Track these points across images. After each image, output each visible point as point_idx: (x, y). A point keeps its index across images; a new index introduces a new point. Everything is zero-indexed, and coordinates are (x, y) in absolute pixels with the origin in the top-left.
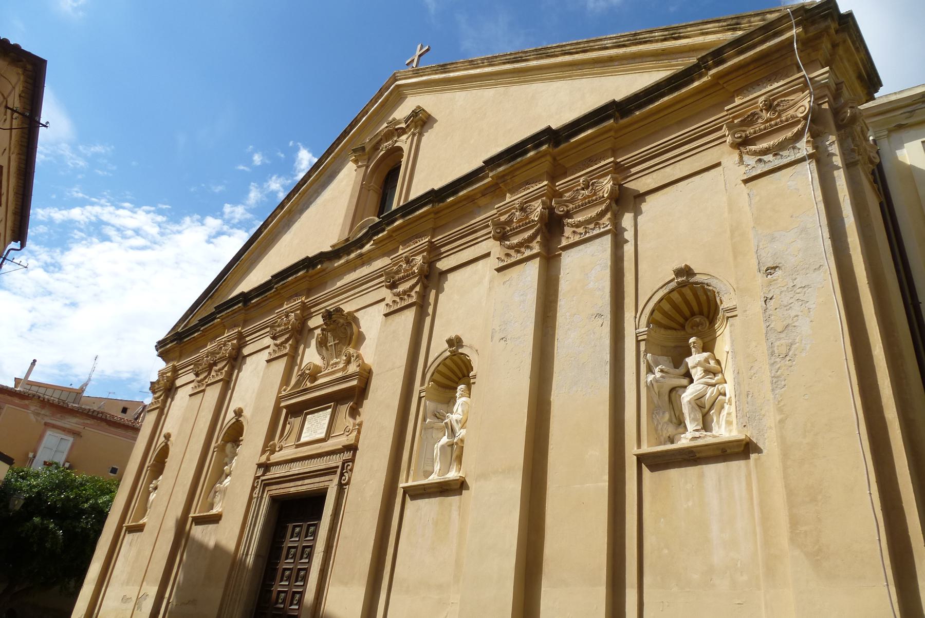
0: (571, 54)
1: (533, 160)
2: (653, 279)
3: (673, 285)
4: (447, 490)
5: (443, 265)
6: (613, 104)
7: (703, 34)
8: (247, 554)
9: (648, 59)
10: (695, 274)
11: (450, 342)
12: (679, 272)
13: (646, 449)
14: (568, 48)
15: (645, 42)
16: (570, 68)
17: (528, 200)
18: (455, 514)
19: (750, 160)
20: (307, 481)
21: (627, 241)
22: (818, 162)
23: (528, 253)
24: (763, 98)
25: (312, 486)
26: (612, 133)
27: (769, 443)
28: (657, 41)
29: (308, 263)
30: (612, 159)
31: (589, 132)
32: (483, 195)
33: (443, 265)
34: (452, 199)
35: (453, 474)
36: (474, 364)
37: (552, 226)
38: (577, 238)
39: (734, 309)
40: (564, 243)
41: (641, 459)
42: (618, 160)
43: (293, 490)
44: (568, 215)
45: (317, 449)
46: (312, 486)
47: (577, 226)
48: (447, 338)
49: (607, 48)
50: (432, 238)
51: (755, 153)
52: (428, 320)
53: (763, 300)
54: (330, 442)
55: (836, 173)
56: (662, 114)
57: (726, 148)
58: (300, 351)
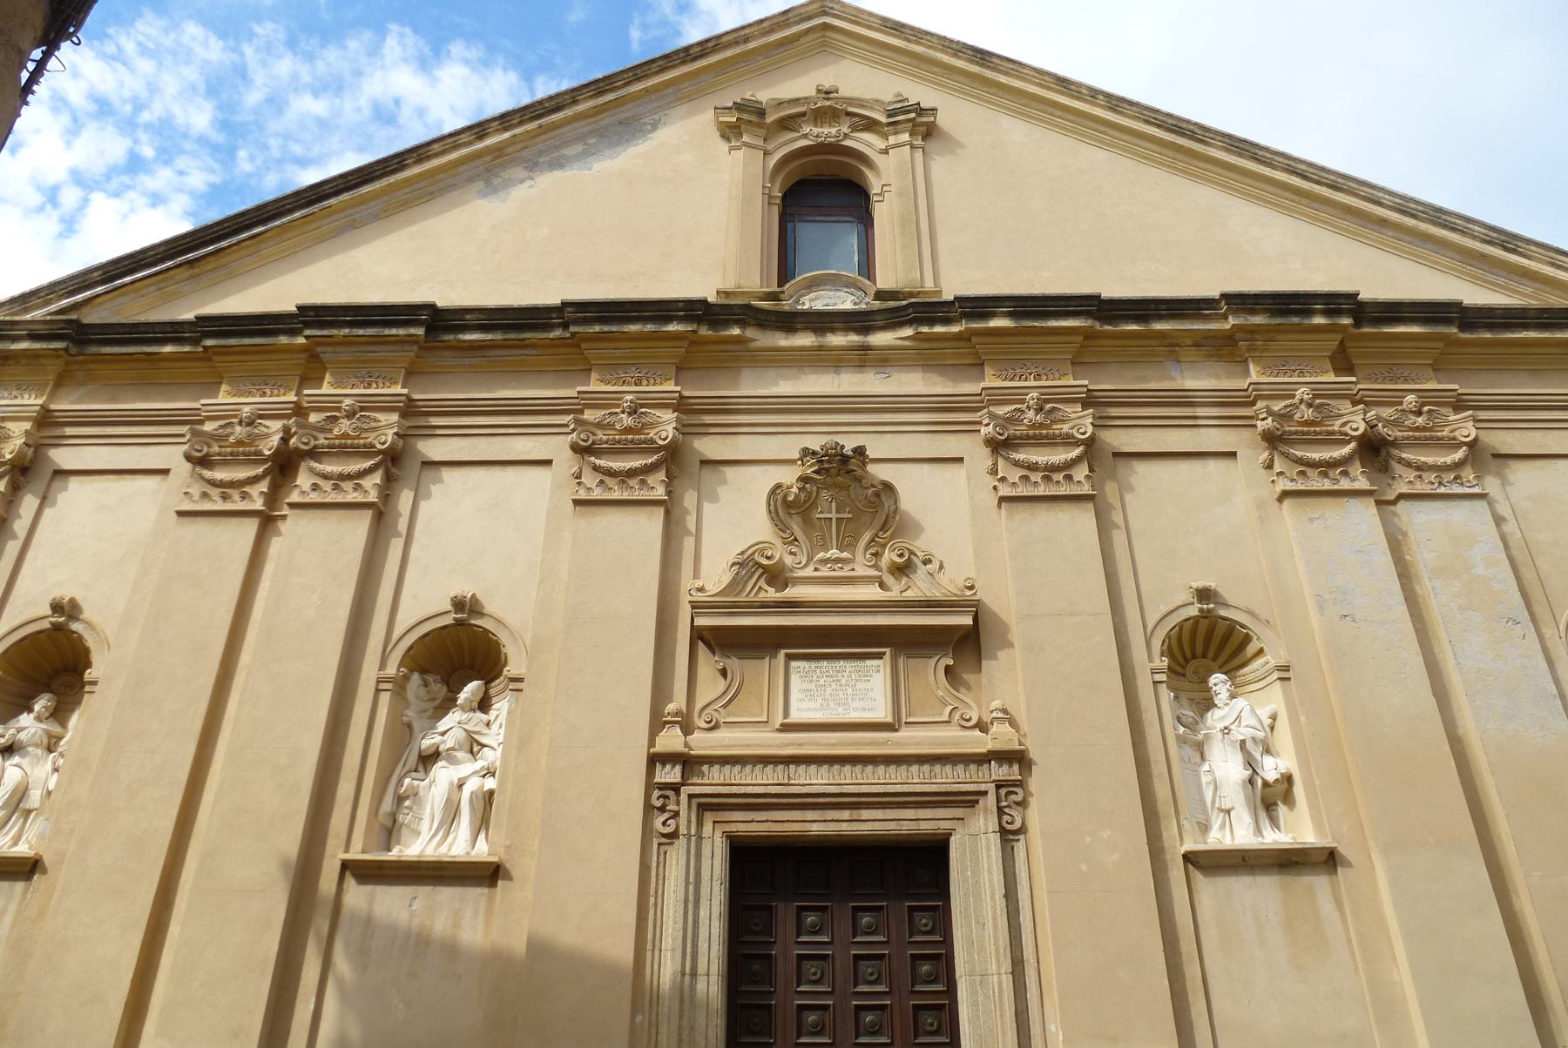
0: (1305, 178)
1: (1318, 329)
2: (422, 599)
3: (45, 625)
4: (1297, 863)
5: (63, 457)
6: (1095, 298)
7: (1553, 265)
8: (694, 974)
9: (1451, 254)
10: (482, 614)
11: (57, 607)
12: (459, 604)
13: (355, 854)
14: (1303, 167)
15: (1453, 229)
16: (1296, 198)
17: (647, 398)
18: (1326, 905)
19: (590, 479)
20: (763, 815)
21: (15, 537)
22: (667, 513)
23: (352, 497)
24: (629, 397)
25: (877, 826)
26: (685, 344)
27: (524, 868)
28: (1474, 238)
29: (438, 322)
30: (405, 391)
31: (1415, 329)
32: (1196, 345)
33: (63, 457)
34: (1135, 327)
35: (482, 851)
36: (95, 658)
37: (284, 465)
38: (314, 497)
39: (520, 680)
40: (295, 497)
41: (346, 866)
42: (416, 397)
43: (816, 829)
44: (314, 454)
45: (872, 743)
46: (877, 826)
47: (326, 477)
48: (453, 594)
49: (1380, 204)
50: (52, 397)
51: (596, 469)
52: (396, 547)
53: (1282, 662)
54: (904, 733)
55: (1115, 532)
56: (1525, 350)
57: (978, 440)
58: (20, 526)
